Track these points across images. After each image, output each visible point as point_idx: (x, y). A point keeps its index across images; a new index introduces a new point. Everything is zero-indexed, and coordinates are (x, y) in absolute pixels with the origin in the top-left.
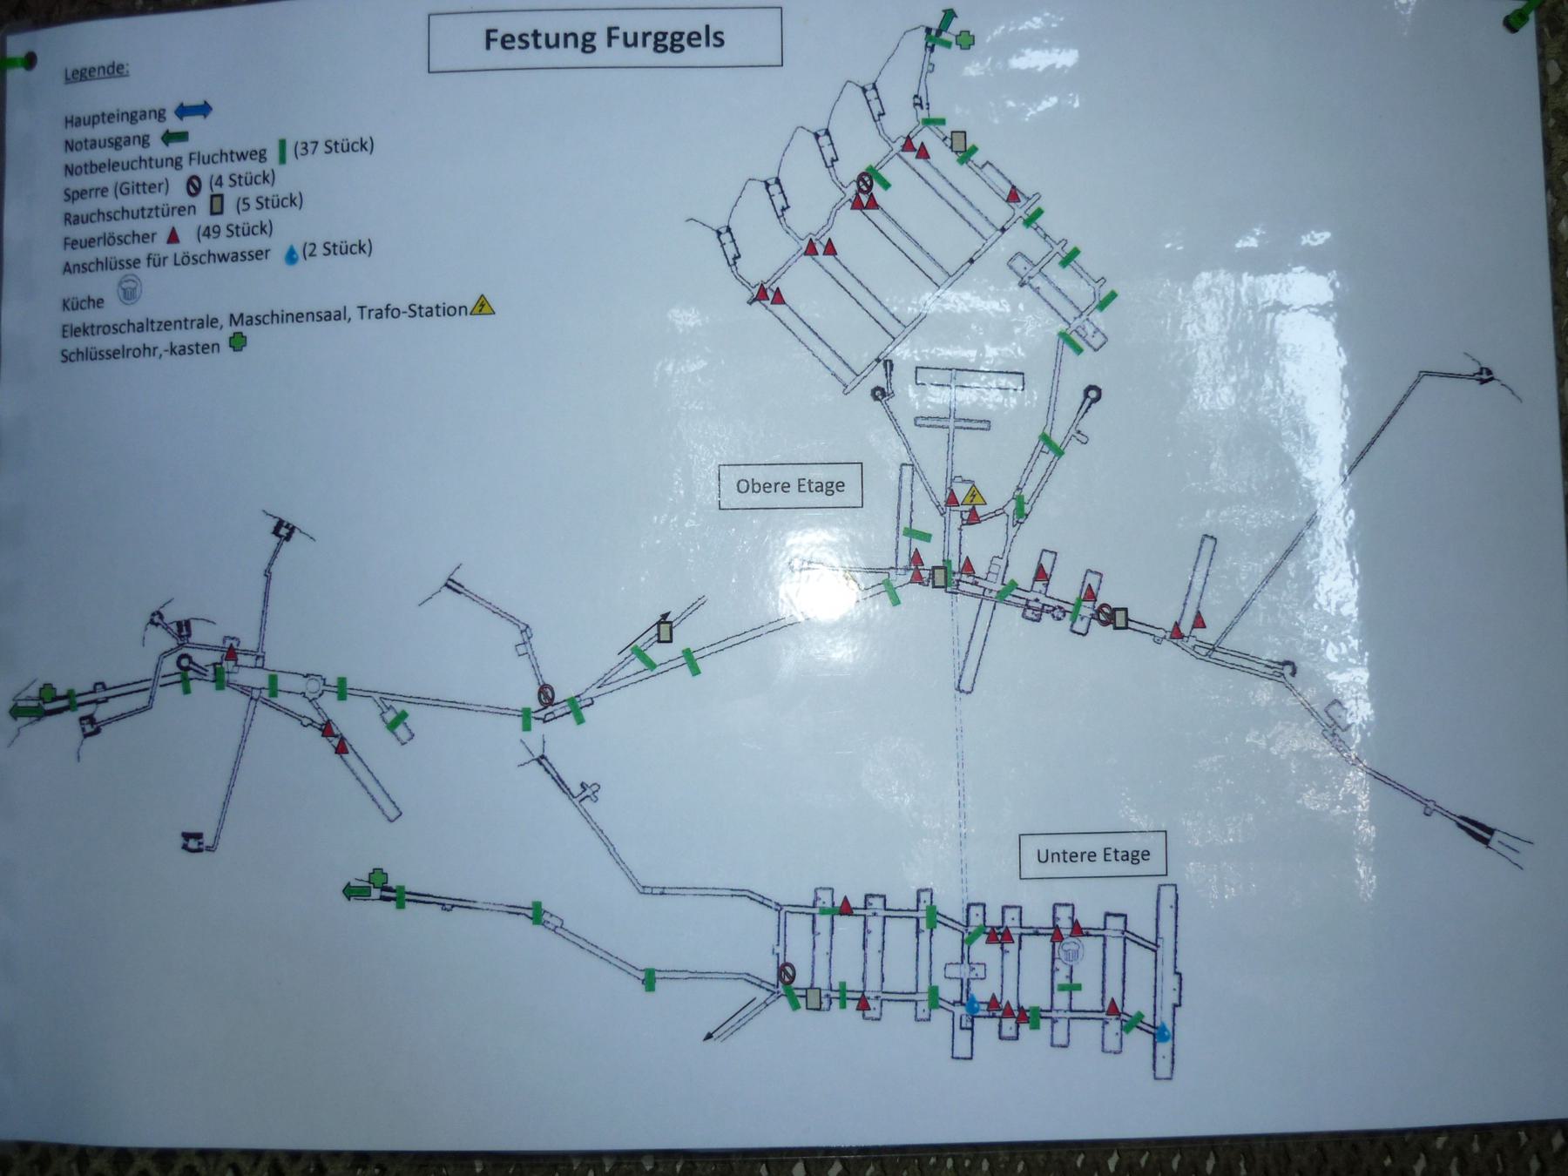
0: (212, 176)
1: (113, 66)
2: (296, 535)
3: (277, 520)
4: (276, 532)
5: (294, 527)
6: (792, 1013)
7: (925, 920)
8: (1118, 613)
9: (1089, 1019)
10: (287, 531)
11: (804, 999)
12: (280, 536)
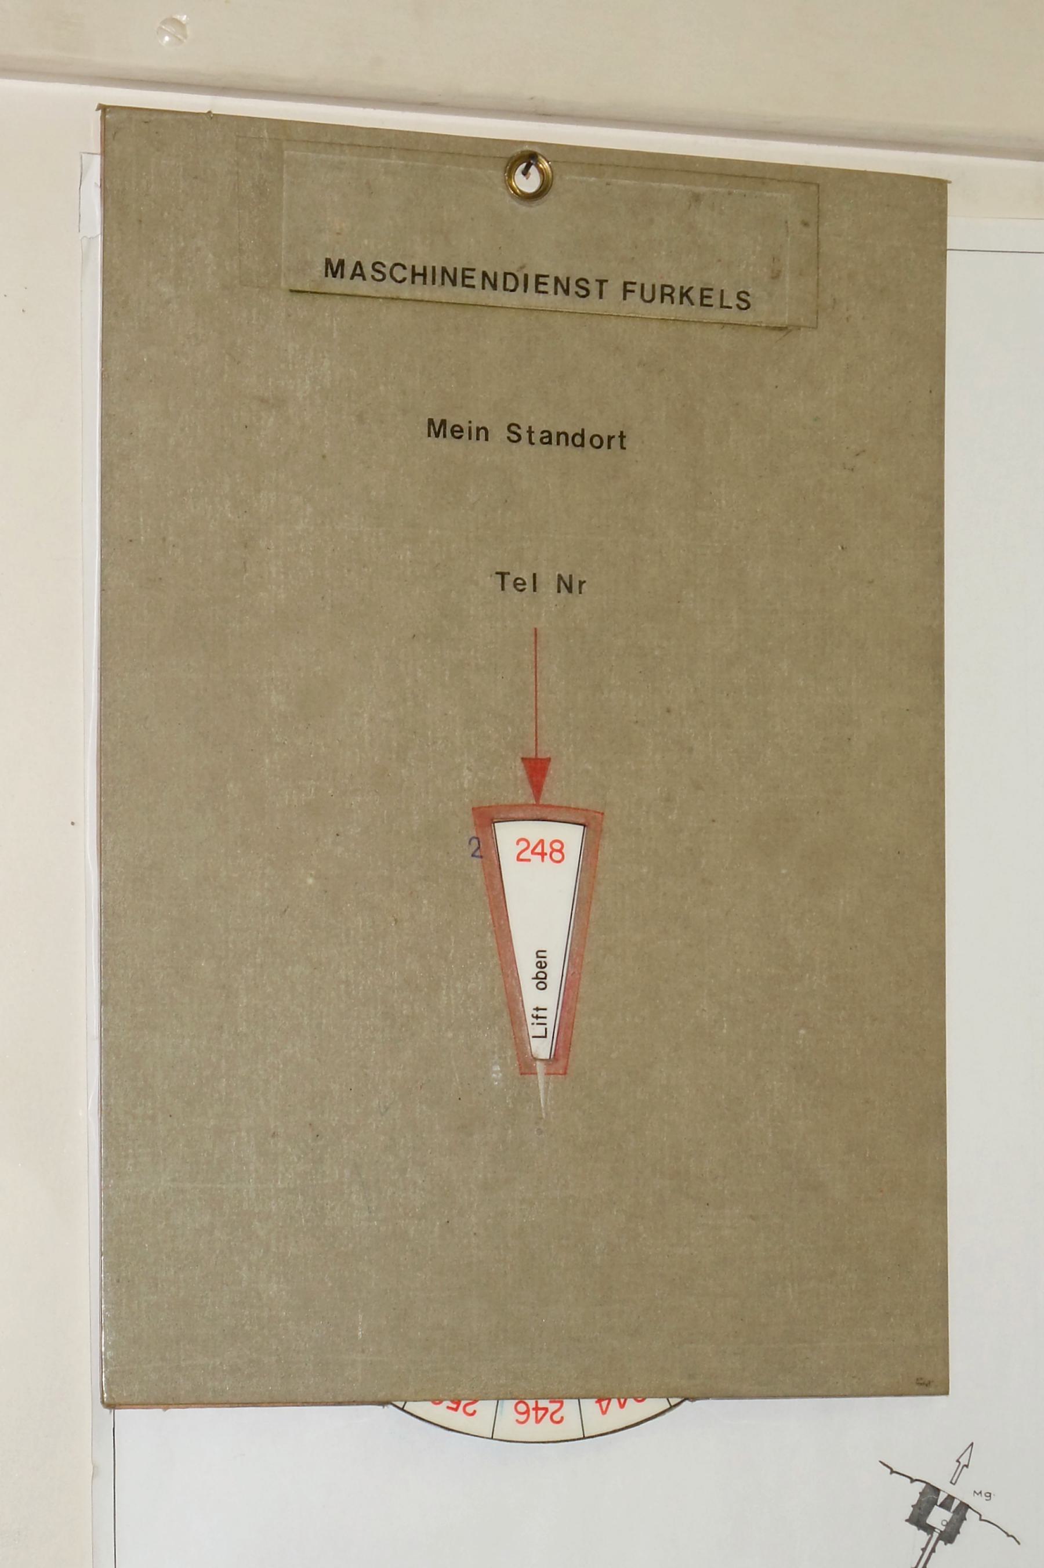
0: (545, 951)
1: (582, 436)
2: (971, 1524)
3: (920, 1487)
4: (918, 1519)
5: (964, 1507)
6: (661, 284)
7: (540, 1401)
8: (579, 444)
9: (572, 910)
10: (947, 1515)
11: (401, 1407)
12: (929, 1529)
